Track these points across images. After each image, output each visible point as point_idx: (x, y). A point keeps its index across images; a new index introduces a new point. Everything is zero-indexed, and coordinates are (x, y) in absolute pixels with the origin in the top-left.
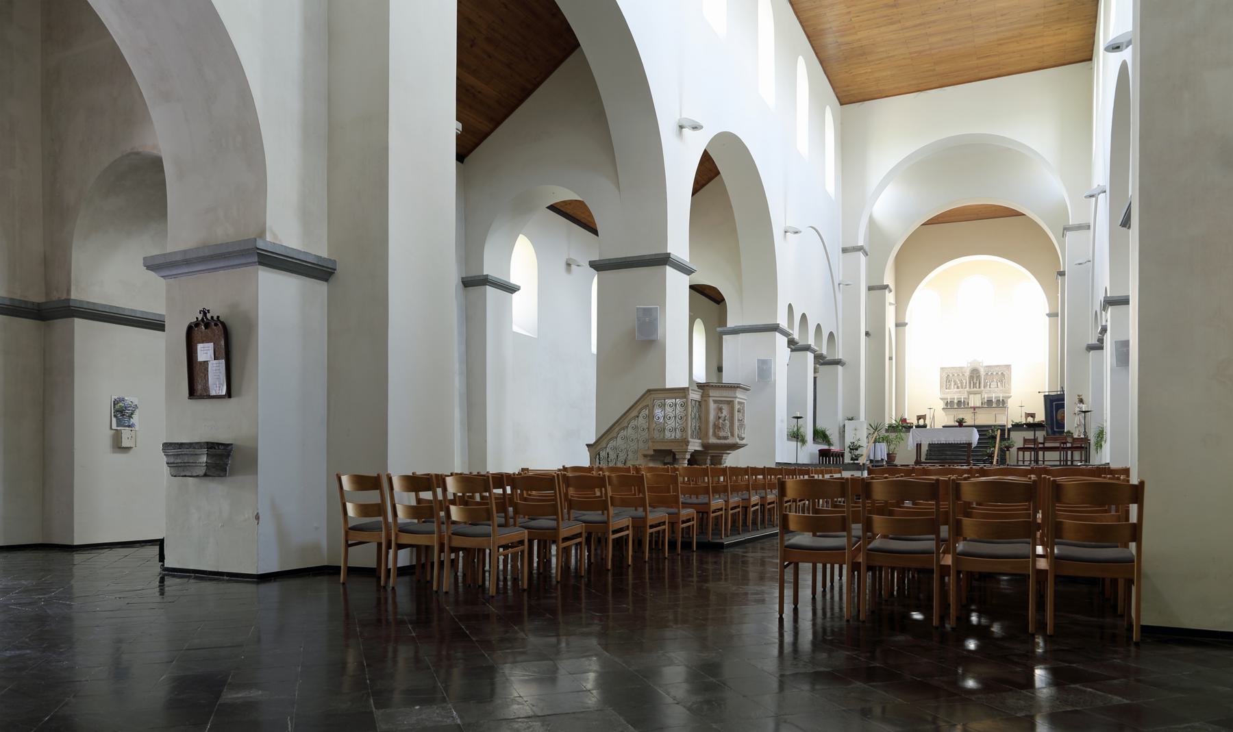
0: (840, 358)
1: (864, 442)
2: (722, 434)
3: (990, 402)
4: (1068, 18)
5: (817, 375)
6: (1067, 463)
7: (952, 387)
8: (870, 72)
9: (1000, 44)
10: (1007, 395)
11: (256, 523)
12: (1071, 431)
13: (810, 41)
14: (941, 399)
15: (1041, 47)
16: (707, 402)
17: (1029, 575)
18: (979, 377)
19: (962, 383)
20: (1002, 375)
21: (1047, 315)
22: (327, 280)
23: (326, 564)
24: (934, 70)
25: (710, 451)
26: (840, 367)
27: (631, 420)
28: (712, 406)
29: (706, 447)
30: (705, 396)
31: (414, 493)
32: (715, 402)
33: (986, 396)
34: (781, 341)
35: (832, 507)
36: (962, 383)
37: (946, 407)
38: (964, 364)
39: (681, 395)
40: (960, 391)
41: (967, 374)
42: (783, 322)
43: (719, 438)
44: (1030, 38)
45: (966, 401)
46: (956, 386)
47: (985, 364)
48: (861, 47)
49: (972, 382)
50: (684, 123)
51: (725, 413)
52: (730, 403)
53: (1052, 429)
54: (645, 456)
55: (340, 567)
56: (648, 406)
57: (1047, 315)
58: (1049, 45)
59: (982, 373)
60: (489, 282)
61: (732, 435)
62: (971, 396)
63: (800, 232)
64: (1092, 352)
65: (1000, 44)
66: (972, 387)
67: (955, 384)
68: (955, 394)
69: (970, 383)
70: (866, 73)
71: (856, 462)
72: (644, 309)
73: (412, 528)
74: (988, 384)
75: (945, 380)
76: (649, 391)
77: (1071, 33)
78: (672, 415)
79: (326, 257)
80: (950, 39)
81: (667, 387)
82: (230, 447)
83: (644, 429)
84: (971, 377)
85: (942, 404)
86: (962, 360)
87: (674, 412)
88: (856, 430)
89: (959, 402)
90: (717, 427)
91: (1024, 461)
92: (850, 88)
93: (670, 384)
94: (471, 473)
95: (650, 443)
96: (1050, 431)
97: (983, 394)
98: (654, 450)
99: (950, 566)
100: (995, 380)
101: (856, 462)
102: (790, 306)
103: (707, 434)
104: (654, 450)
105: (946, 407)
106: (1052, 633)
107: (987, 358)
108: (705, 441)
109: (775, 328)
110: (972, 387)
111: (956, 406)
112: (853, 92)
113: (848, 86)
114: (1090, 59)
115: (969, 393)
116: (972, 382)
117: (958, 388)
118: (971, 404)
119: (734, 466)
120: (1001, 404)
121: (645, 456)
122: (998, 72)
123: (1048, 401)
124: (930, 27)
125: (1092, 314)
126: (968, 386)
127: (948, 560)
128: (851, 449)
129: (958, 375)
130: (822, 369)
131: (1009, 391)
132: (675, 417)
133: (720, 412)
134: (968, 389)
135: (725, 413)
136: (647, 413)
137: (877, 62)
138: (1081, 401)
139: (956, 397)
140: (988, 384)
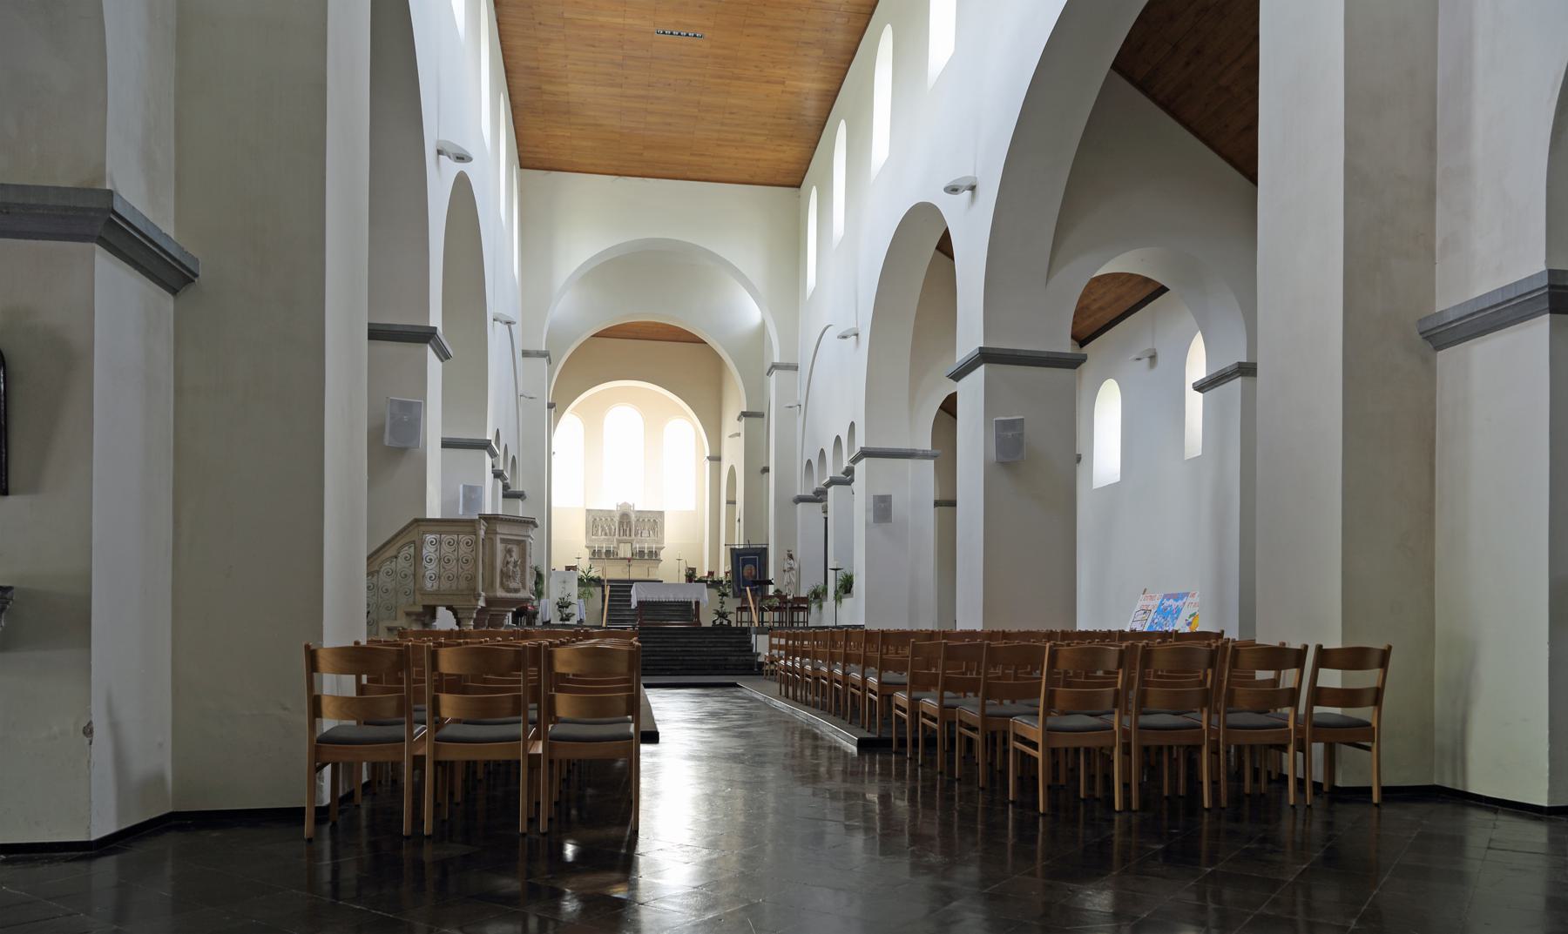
0: (521, 490)
1: (574, 599)
2: (513, 585)
3: (641, 553)
4: (792, 136)
5: (824, 515)
6: (792, 625)
8: (568, 137)
9: (719, 145)
10: (659, 546)
11: (88, 742)
12: (781, 590)
13: (507, 77)
14: (587, 547)
15: (758, 160)
16: (492, 541)
17: (519, 762)
18: (629, 523)
19: (610, 529)
20: (654, 521)
21: (708, 458)
22: (174, 292)
23: (171, 810)
24: (641, 154)
25: (493, 609)
27: (383, 562)
28: (500, 547)
31: (354, 676)
32: (503, 541)
33: (638, 546)
35: (386, 684)
36: (610, 529)
37: (592, 557)
38: (614, 508)
39: (468, 529)
40: (608, 539)
41: (617, 519)
42: (490, 436)
43: (509, 590)
44: (750, 147)
45: (615, 550)
46: (603, 533)
47: (636, 509)
48: (568, 103)
49: (621, 529)
50: (447, 148)
51: (515, 556)
52: (521, 544)
53: (739, 586)
54: (408, 614)
55: (304, 808)
56: (414, 542)
57: (708, 458)
58: (766, 160)
60: (1236, 372)
62: (622, 545)
63: (515, 323)
64: (800, 505)
65: (719, 145)
66: (622, 533)
67: (602, 531)
68: (603, 543)
70: (564, 136)
71: (567, 623)
72: (402, 403)
73: (344, 734)
76: (416, 521)
77: (790, 153)
78: (453, 557)
80: (670, 124)
81: (428, 517)
82: (9, 593)
83: (406, 575)
84: (621, 523)
85: (586, 554)
86: (609, 502)
87: (456, 553)
88: (564, 582)
89: (608, 552)
90: (505, 575)
91: (798, 622)
92: (537, 150)
93: (429, 516)
94: (357, 643)
95: (418, 597)
96: (736, 589)
97: (634, 543)
98: (424, 606)
99: (540, 755)
101: (567, 623)
103: (492, 584)
104: (424, 606)
105: (592, 557)
106: (546, 830)
107: (642, 502)
108: (491, 594)
109: (425, 336)
110: (622, 533)
111: (604, 556)
112: (542, 156)
113: (537, 146)
114: (798, 186)
115: (619, 542)
116: (621, 529)
117: (606, 534)
118: (621, 555)
119: (1091, 630)
120: (654, 556)
121: (408, 614)
122: (577, 169)
123: (735, 556)
124: (652, 104)
126: (617, 533)
127: (539, 748)
128: (560, 607)
132: (458, 560)
133: (508, 556)
134: (617, 536)
135: (515, 556)
136: (413, 554)
137: (579, 127)
138: (791, 557)
139: (654, 546)
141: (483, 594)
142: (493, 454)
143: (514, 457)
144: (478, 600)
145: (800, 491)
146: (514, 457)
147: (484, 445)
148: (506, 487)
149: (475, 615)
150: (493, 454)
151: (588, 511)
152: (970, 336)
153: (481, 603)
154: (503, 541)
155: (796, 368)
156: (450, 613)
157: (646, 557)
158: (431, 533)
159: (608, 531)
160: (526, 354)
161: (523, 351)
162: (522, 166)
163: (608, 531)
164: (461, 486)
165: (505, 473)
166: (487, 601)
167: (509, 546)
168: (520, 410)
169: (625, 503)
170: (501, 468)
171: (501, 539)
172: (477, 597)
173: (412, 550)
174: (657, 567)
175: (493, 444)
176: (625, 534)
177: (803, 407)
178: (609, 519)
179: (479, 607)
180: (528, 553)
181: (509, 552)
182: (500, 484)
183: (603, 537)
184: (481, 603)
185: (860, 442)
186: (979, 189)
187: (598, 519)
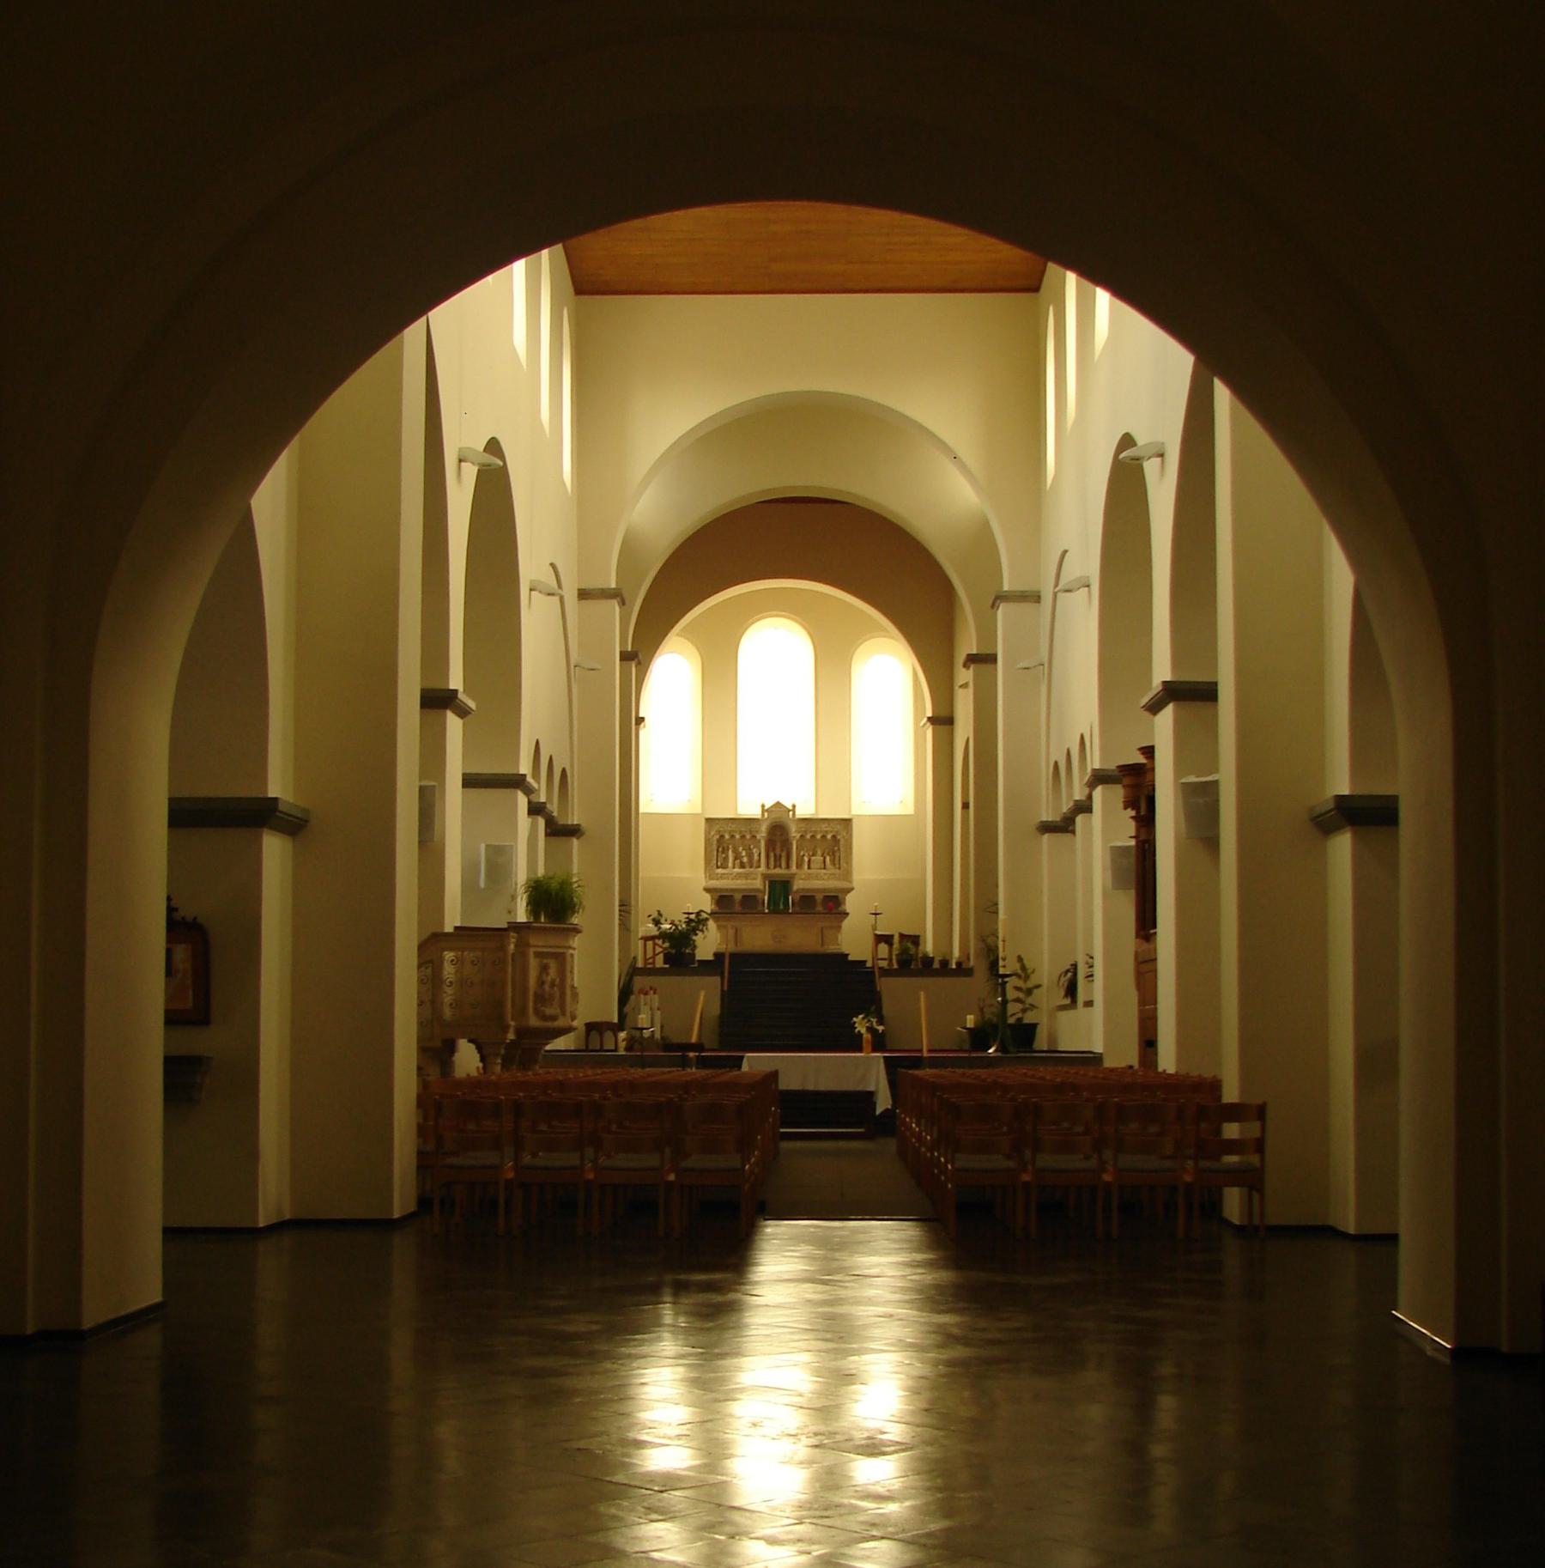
0: (575, 823)
2: (548, 1011)
7: (730, 864)
14: (707, 890)
16: (524, 955)
18: (786, 844)
19: (750, 855)
26: (575, 841)
28: (533, 963)
29: (522, 1032)
30: (522, 945)
32: (538, 955)
34: (522, 801)
36: (750, 855)
38: (755, 812)
41: (762, 833)
42: (525, 768)
43: (545, 1018)
49: (772, 855)
56: (431, 962)
57: (929, 718)
59: (794, 833)
61: (563, 1013)
64: (1046, 835)
67: (736, 859)
68: (734, 879)
69: (768, 857)
74: (806, 859)
75: (715, 847)
79: (291, 801)
84: (770, 844)
90: (541, 999)
100: (819, 853)
102: (537, 742)
114: (1036, 289)
116: (772, 855)
117: (742, 866)
120: (832, 905)
125: (1048, 766)
129: (743, 837)
130: (556, 841)
131: (848, 875)
134: (763, 869)
135: (553, 973)
140: (806, 859)
141: (512, 1023)
142: (528, 791)
143: (564, 770)
144: (507, 1032)
145: (1047, 816)
146: (564, 770)
147: (517, 782)
148: (550, 822)
149: (503, 1052)
150: (528, 791)
151: (708, 820)
152: (1162, 671)
153: (511, 1036)
154: (538, 955)
155: (1036, 598)
156: (472, 1046)
157: (819, 908)
158: (450, 949)
159: (745, 860)
160: (583, 594)
161: (579, 590)
162: (580, 290)
163: (745, 860)
164: (483, 846)
165: (548, 806)
166: (519, 1032)
167: (545, 961)
168: (575, 690)
169: (778, 804)
170: (543, 799)
171: (535, 953)
172: (505, 1028)
173: (429, 970)
174: (840, 927)
175: (529, 779)
176: (777, 865)
177: (1046, 666)
178: (748, 837)
179: (508, 1041)
180: (568, 968)
181: (544, 969)
182: (541, 822)
183: (737, 870)
184: (511, 1036)
185: (1095, 762)
186: (1166, 456)
187: (727, 837)
